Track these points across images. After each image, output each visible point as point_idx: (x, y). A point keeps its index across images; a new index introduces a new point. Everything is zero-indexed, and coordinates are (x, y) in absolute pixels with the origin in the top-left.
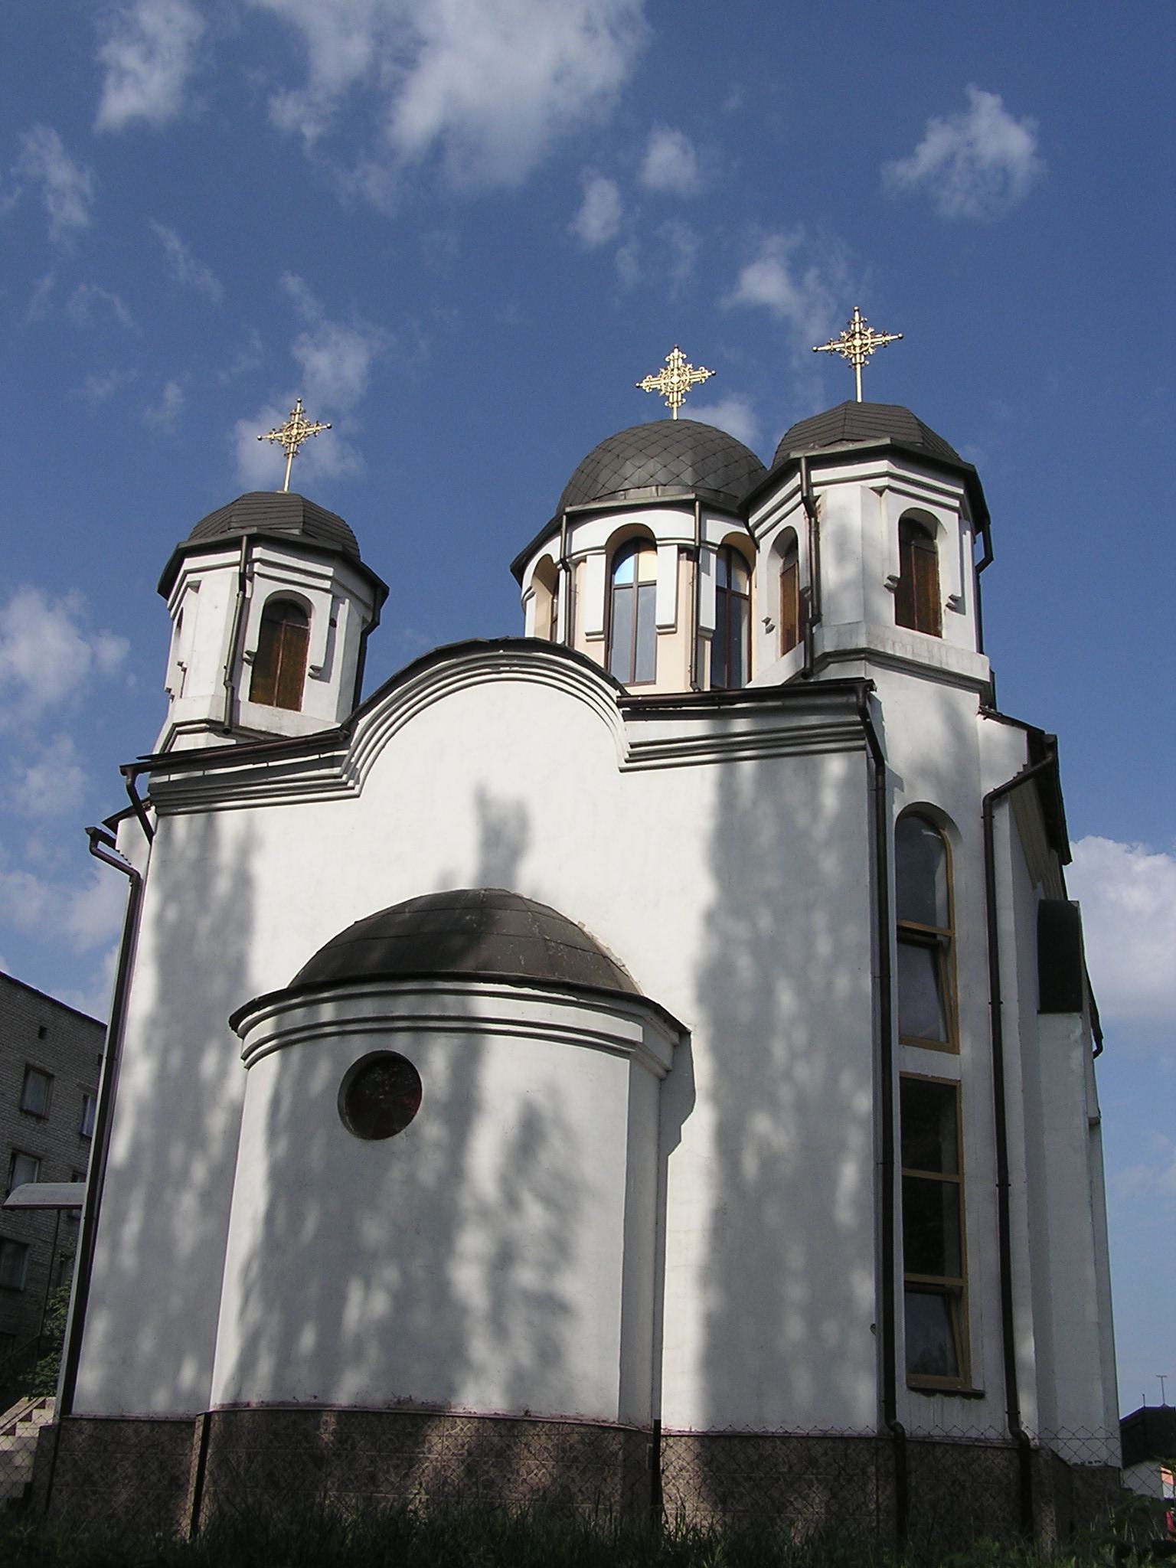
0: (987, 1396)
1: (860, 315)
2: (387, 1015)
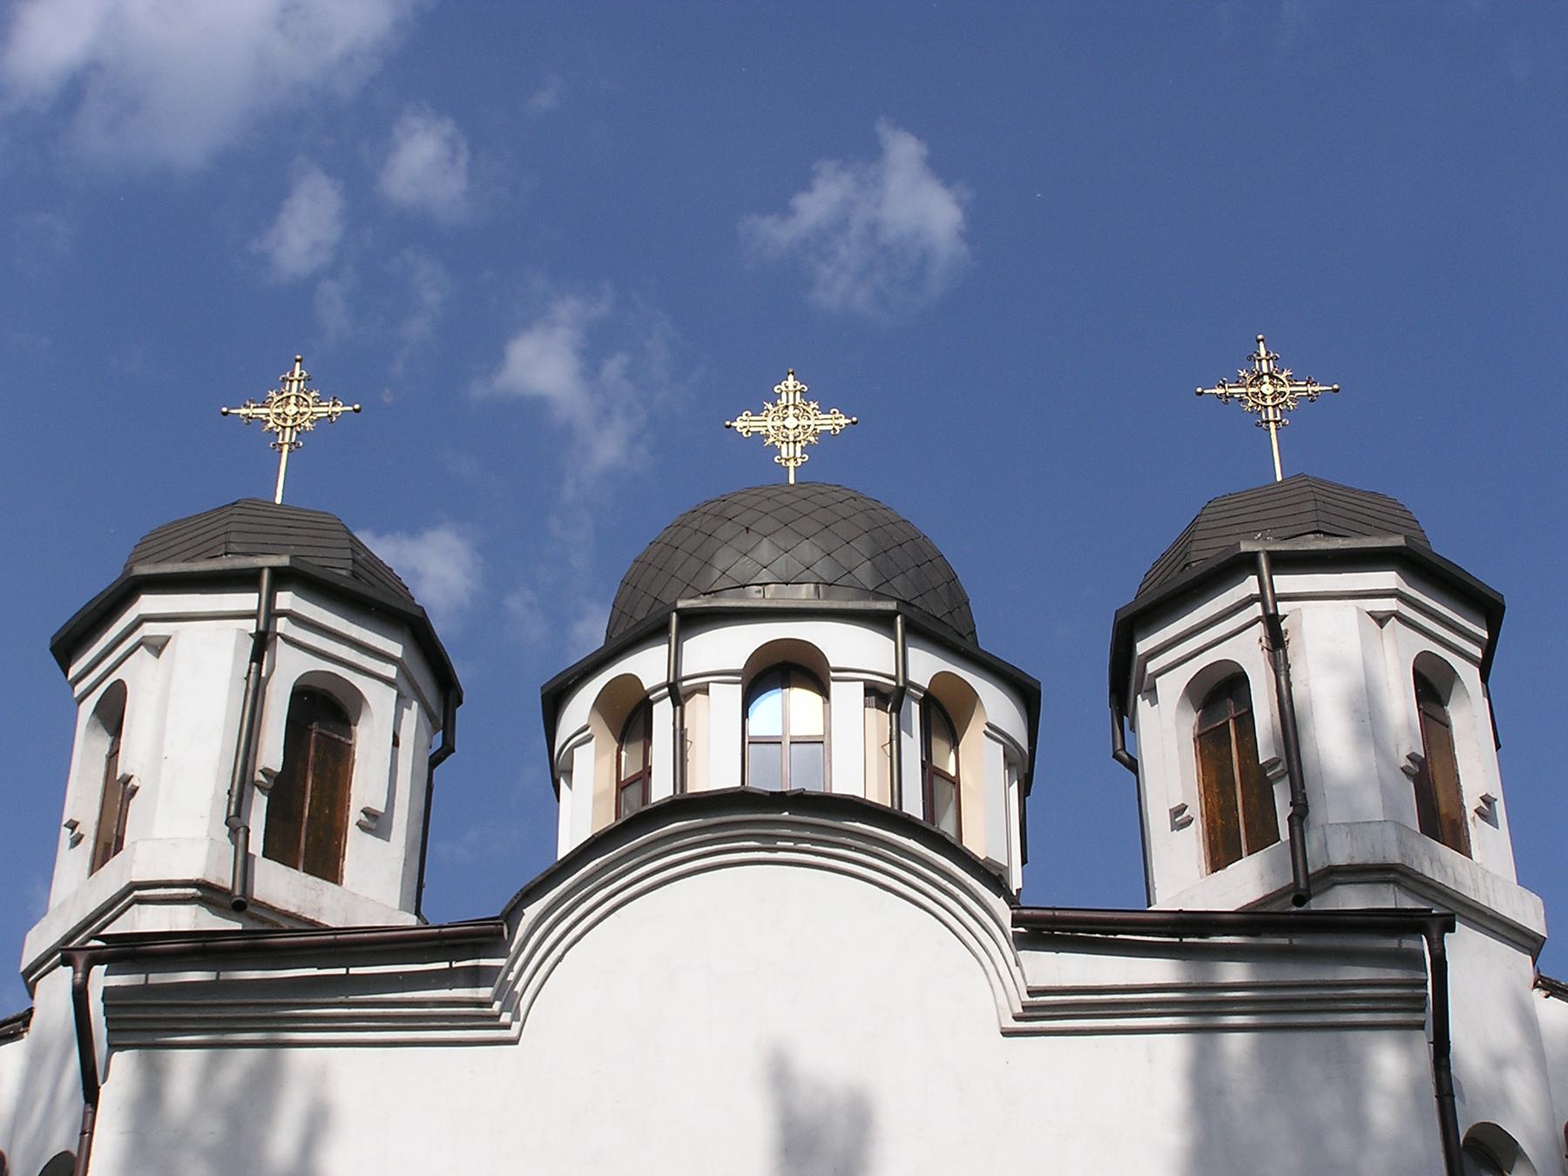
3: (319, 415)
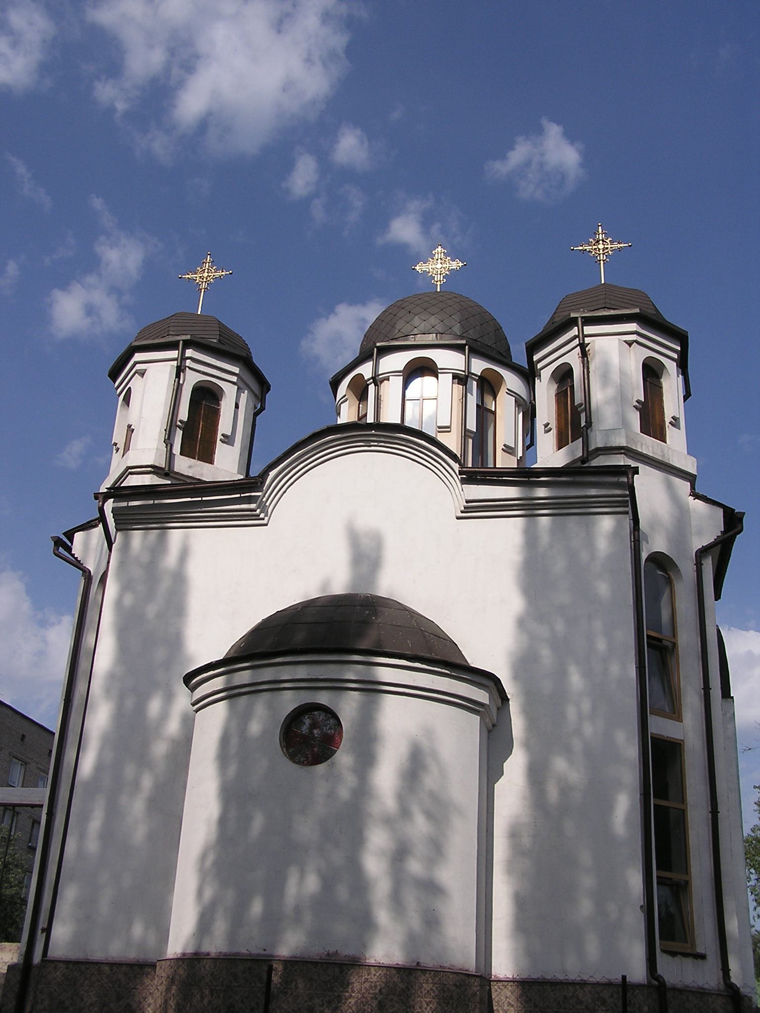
0: (708, 957)
1: (602, 229)
2: (319, 677)
3: (216, 276)
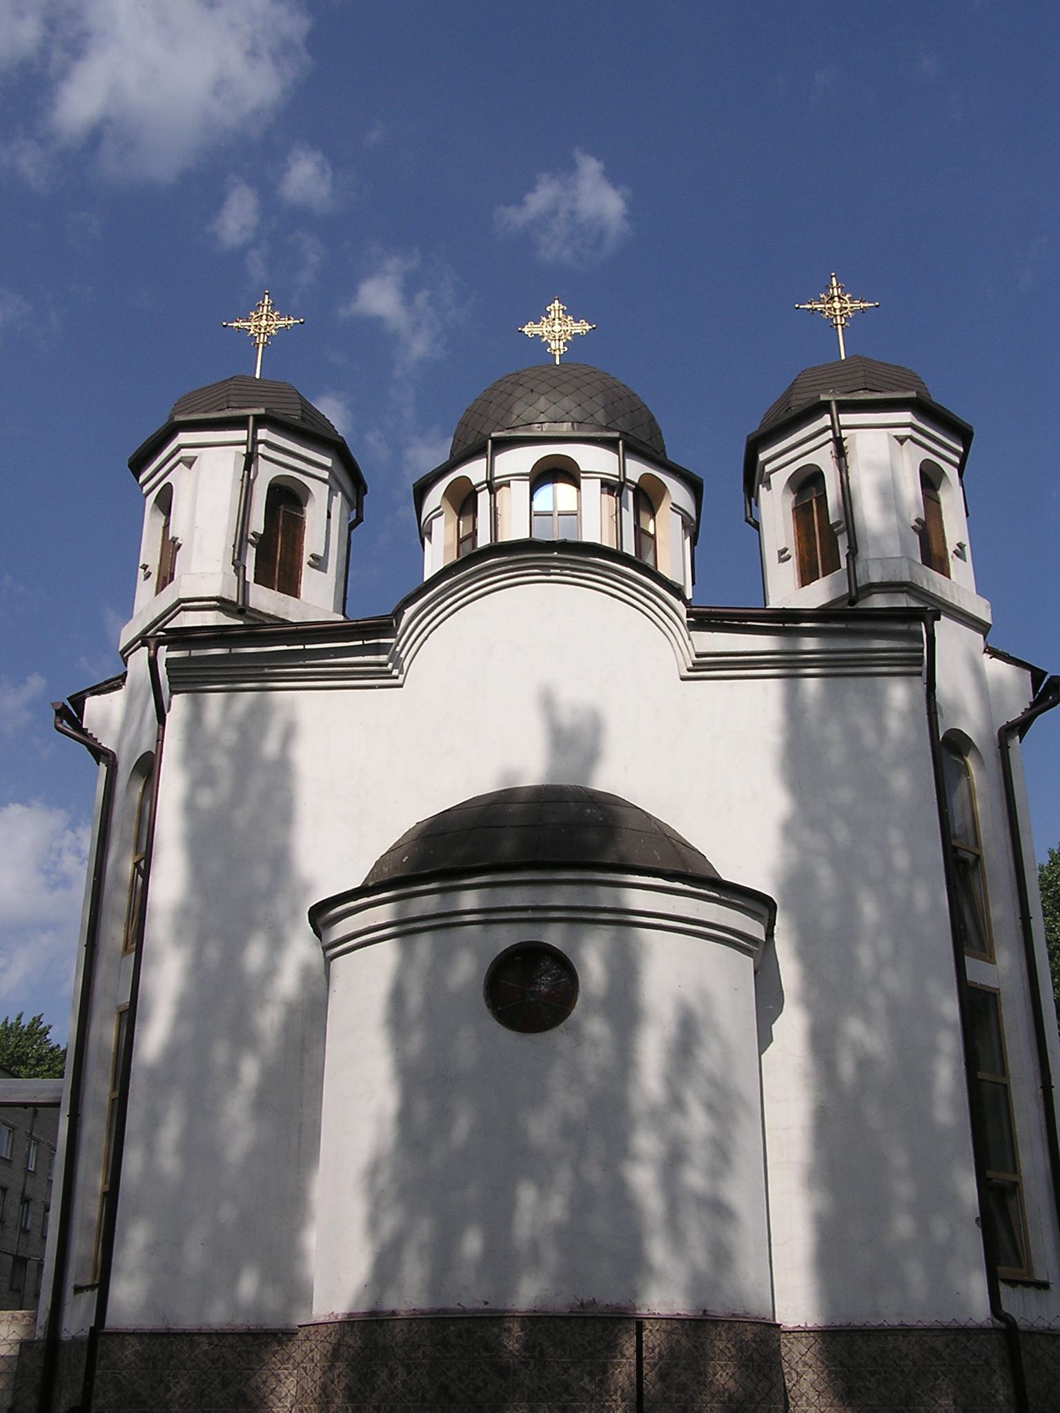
1: (836, 280)
3: (280, 326)
